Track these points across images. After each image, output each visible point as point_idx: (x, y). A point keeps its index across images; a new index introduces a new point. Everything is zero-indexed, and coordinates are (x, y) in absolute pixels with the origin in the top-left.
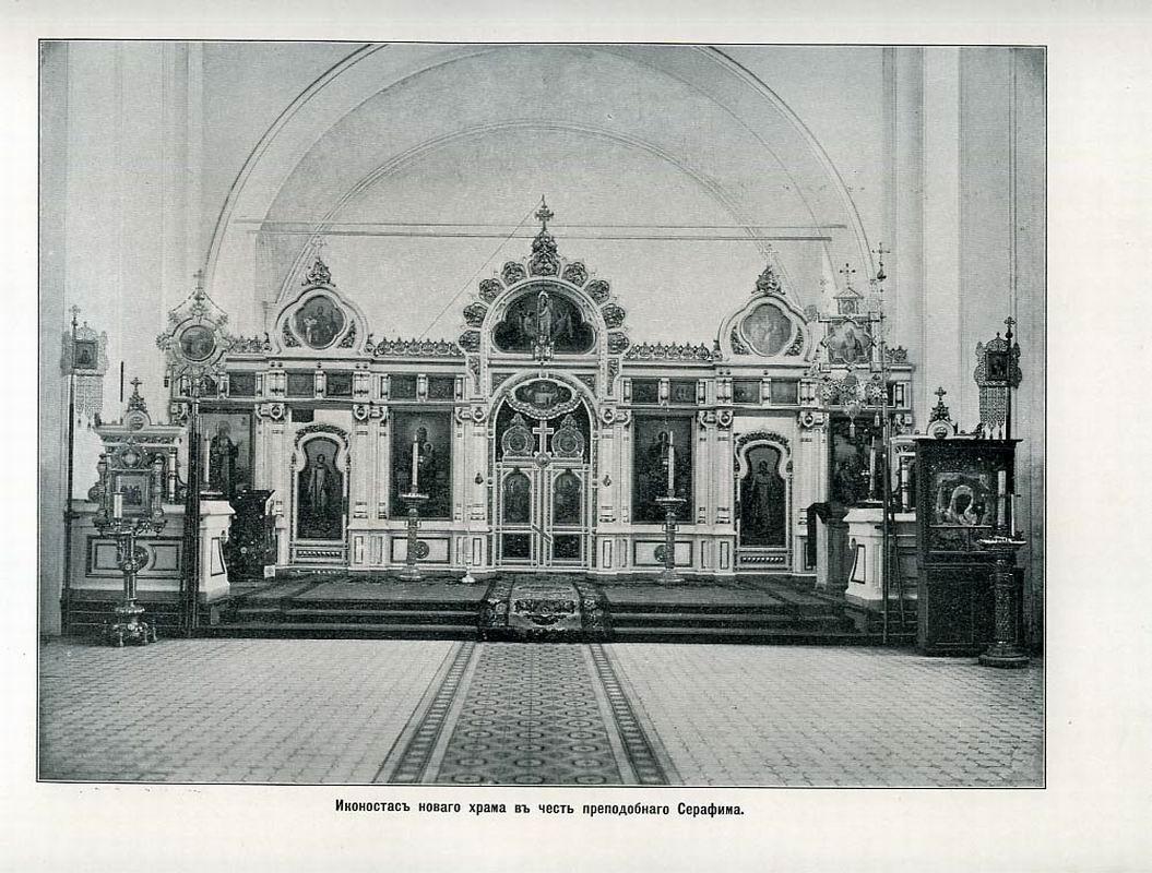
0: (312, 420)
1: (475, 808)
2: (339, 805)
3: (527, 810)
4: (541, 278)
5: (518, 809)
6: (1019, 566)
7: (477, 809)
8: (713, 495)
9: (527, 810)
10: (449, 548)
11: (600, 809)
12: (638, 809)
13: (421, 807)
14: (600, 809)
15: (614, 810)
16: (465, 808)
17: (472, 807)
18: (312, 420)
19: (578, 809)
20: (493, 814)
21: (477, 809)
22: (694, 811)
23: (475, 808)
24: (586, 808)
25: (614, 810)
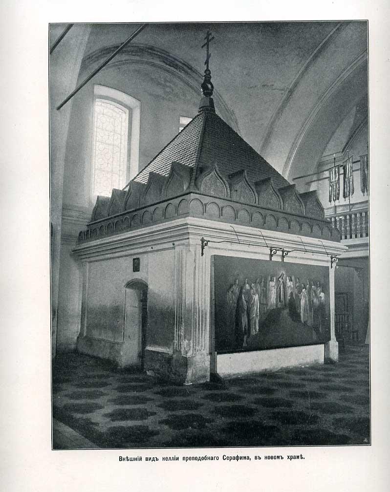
0: (134, 259)
1: (290, 457)
2: (121, 459)
3: (260, 458)
4: (138, 423)
5: (256, 458)
6: (105, 407)
7: (290, 458)
8: (140, 423)
9: (260, 458)
10: (84, 84)
11: (190, 459)
12: (205, 458)
13: (266, 458)
14: (190, 459)
15: (196, 459)
16: (181, 459)
17: (288, 457)
18: (134, 259)
19: (160, 459)
20: (297, 460)
21: (290, 458)
22: (230, 459)
23: (290, 457)
24: (184, 458)
25: (196, 459)
